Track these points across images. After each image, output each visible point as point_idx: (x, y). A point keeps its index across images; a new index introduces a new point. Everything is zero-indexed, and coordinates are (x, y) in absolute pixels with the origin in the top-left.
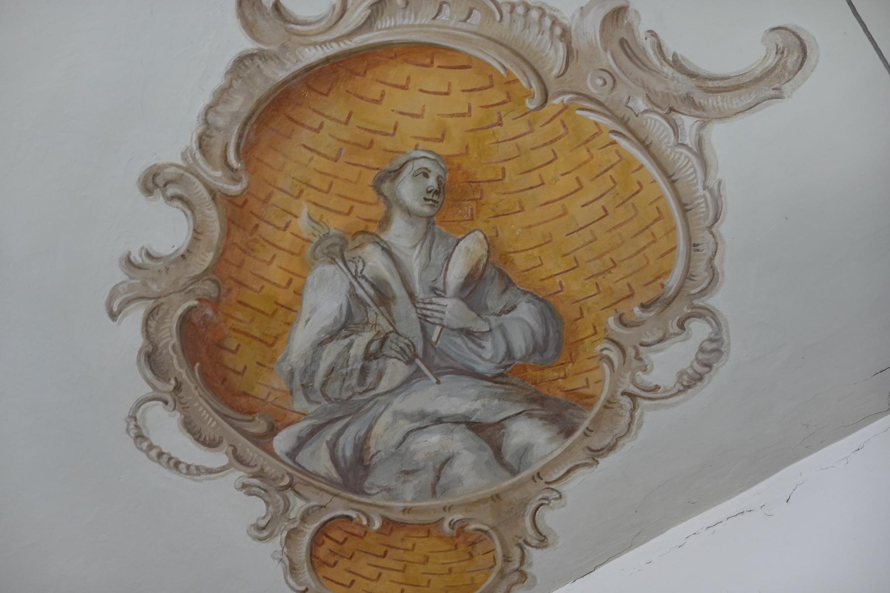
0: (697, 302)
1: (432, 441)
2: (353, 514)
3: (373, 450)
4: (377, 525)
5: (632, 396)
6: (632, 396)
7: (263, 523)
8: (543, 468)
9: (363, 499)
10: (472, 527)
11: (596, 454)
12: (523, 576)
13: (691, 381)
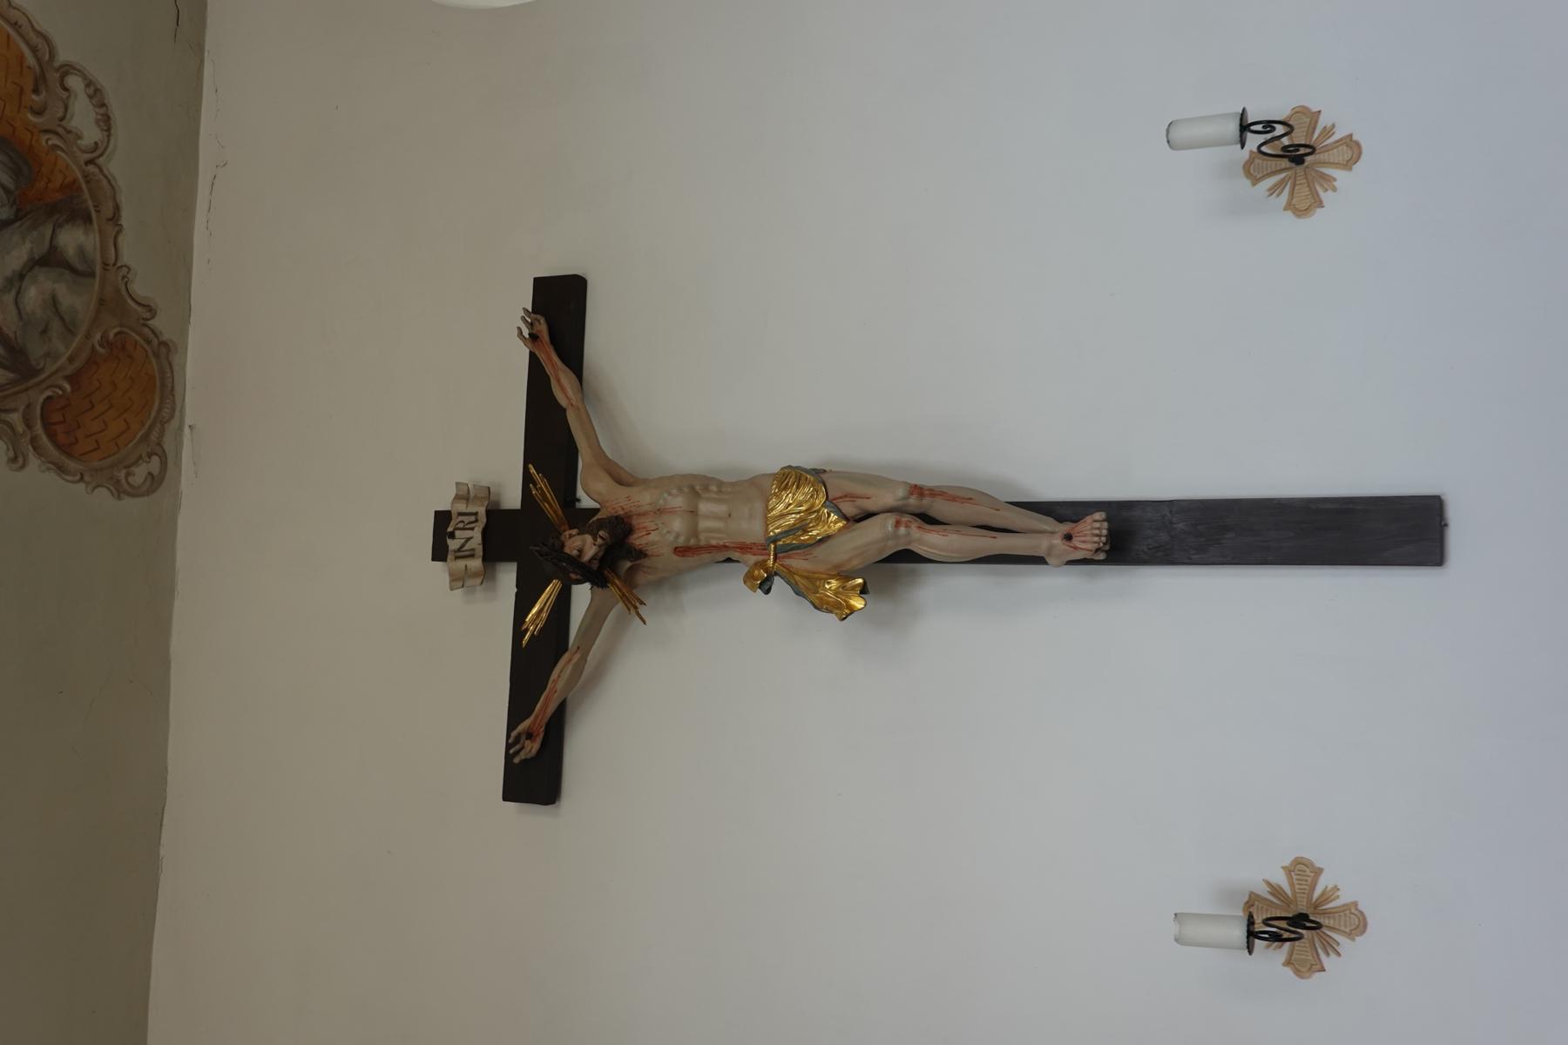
0: (56, 64)
1: (33, 295)
2: (48, 393)
3: (12, 335)
4: (68, 387)
5: (91, 162)
6: (91, 162)
7: (11, 454)
8: (102, 256)
9: (43, 376)
10: (111, 335)
11: (115, 218)
12: (164, 344)
13: (106, 122)
